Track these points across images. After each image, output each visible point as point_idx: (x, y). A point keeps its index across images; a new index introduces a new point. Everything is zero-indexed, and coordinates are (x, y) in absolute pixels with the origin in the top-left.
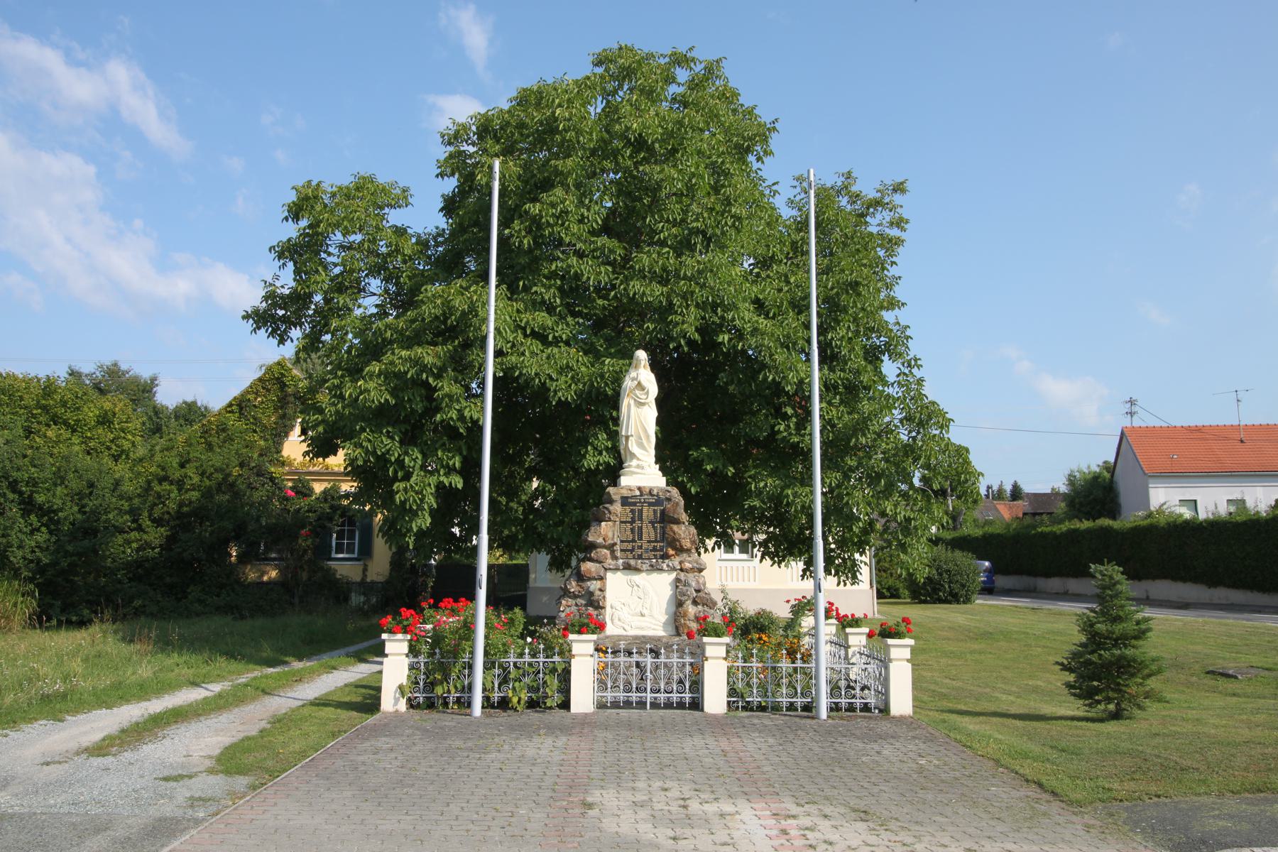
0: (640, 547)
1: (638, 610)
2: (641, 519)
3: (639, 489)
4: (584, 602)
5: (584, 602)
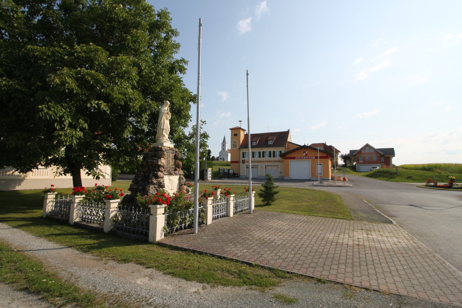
0: (169, 167)
1: (171, 188)
2: (169, 158)
3: (169, 147)
4: (157, 186)
5: (157, 186)
